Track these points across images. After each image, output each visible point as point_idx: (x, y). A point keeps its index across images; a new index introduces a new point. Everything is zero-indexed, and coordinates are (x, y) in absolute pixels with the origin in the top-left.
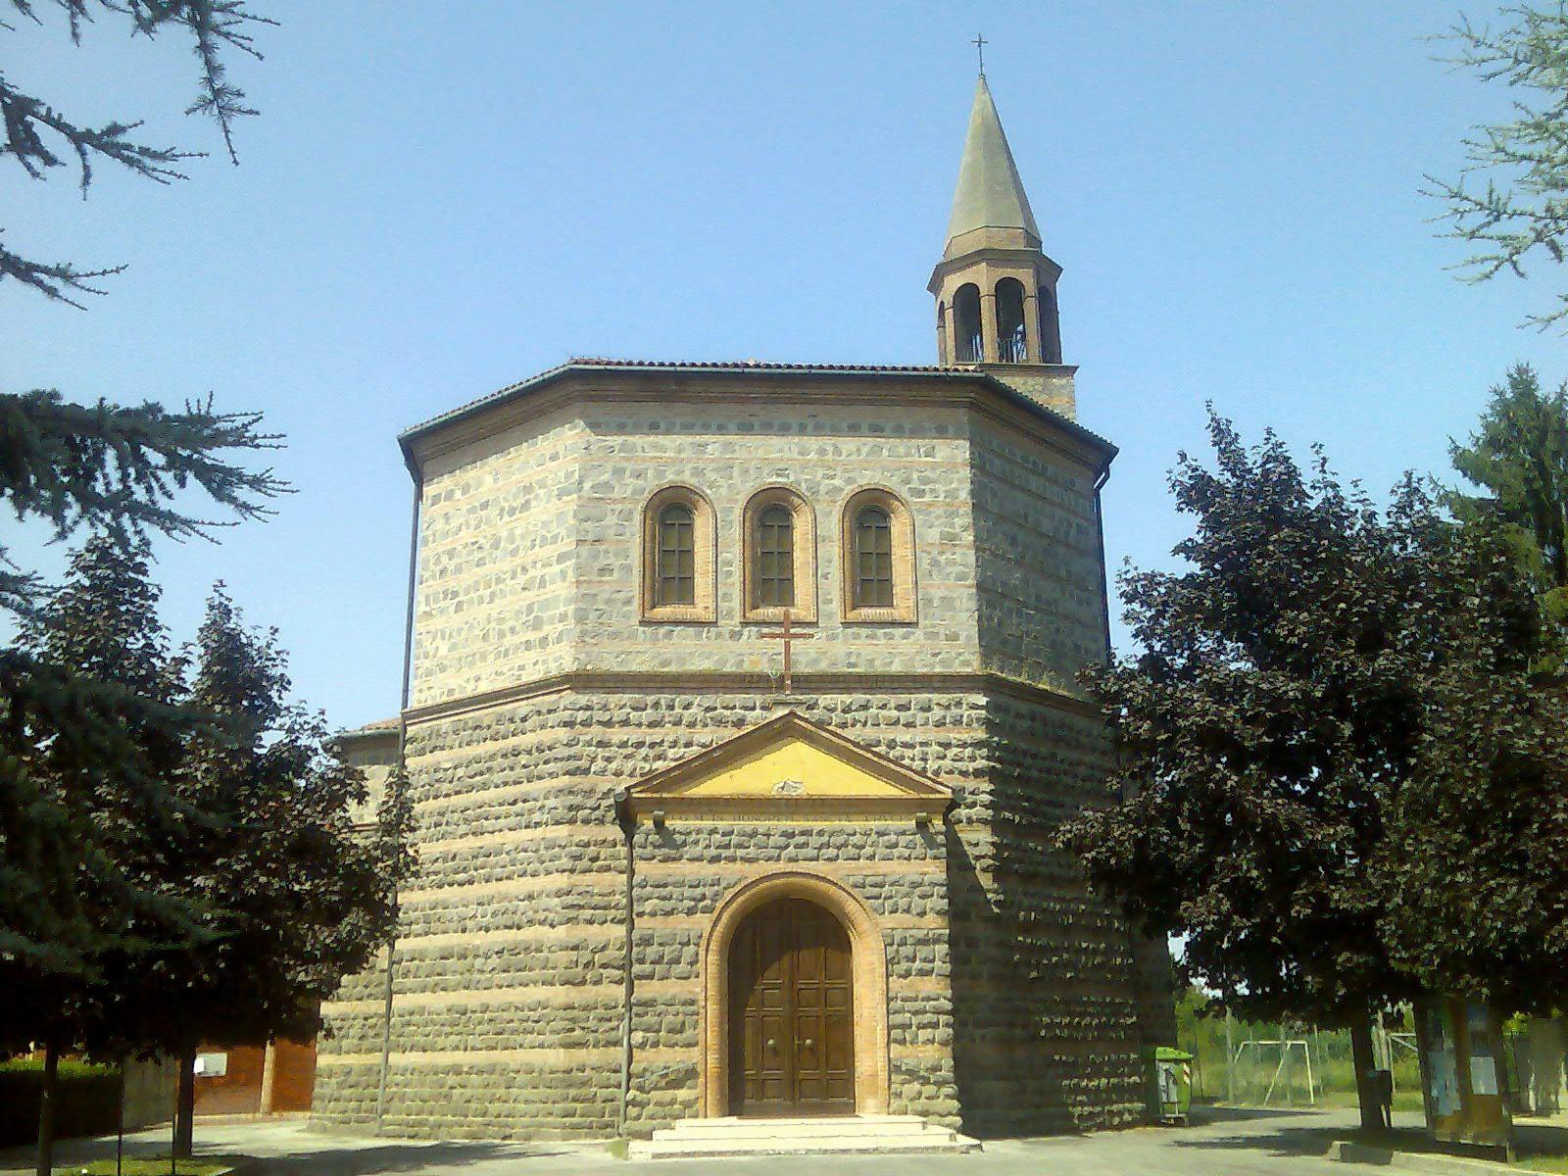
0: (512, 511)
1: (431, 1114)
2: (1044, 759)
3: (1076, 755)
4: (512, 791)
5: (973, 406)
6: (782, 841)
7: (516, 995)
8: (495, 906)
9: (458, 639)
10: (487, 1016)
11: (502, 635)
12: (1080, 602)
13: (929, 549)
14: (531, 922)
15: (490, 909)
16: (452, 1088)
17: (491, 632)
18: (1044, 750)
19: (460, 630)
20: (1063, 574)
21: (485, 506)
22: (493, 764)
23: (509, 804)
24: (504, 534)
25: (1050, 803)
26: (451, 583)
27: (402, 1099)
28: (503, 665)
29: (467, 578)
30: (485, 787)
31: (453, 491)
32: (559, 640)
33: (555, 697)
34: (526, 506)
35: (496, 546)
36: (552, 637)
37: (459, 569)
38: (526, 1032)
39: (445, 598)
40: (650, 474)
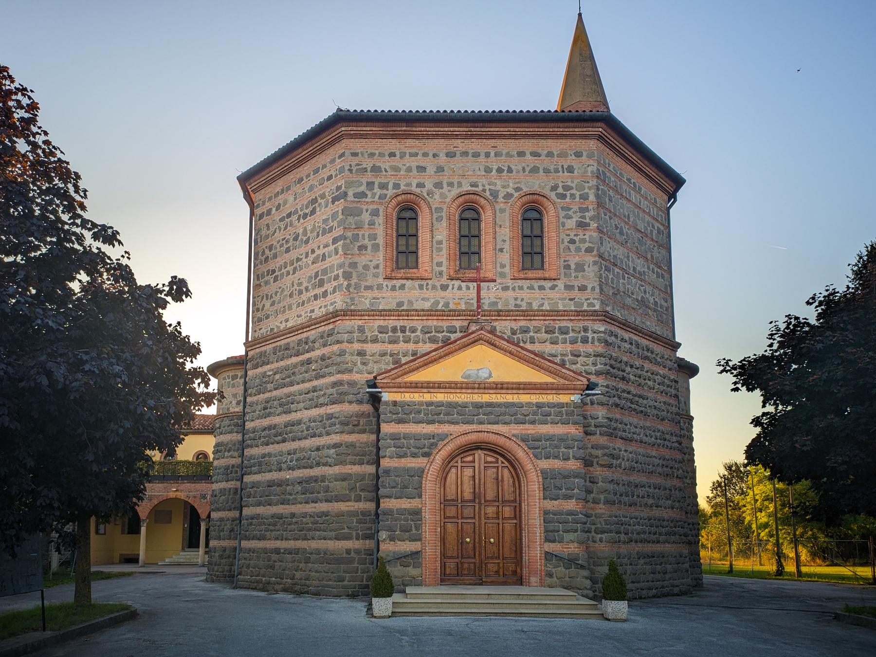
0: (305, 216)
1: (264, 576)
2: (637, 368)
3: (655, 368)
4: (308, 385)
5: (600, 138)
6: (475, 411)
7: (309, 508)
8: (298, 455)
9: (276, 298)
10: (294, 520)
11: (300, 292)
12: (658, 277)
13: (568, 232)
14: (318, 464)
15: (295, 457)
16: (275, 561)
17: (294, 292)
18: (638, 363)
19: (276, 293)
20: (649, 257)
21: (289, 215)
22: (296, 370)
23: (306, 394)
24: (301, 231)
25: (640, 396)
26: (271, 266)
27: (248, 567)
28: (302, 311)
29: (280, 261)
30: (291, 384)
31: (271, 209)
32: (334, 291)
33: (331, 326)
34: (313, 212)
35: (296, 239)
36: (330, 290)
37: (275, 256)
38: (316, 530)
39: (268, 275)
40: (391, 186)
